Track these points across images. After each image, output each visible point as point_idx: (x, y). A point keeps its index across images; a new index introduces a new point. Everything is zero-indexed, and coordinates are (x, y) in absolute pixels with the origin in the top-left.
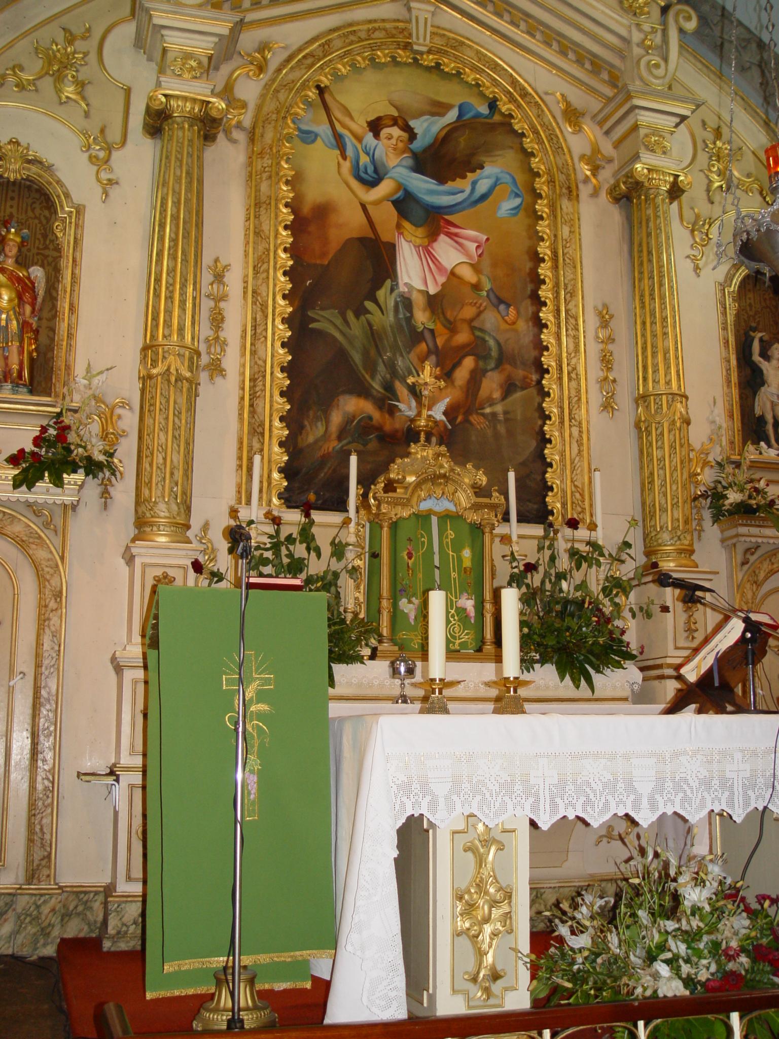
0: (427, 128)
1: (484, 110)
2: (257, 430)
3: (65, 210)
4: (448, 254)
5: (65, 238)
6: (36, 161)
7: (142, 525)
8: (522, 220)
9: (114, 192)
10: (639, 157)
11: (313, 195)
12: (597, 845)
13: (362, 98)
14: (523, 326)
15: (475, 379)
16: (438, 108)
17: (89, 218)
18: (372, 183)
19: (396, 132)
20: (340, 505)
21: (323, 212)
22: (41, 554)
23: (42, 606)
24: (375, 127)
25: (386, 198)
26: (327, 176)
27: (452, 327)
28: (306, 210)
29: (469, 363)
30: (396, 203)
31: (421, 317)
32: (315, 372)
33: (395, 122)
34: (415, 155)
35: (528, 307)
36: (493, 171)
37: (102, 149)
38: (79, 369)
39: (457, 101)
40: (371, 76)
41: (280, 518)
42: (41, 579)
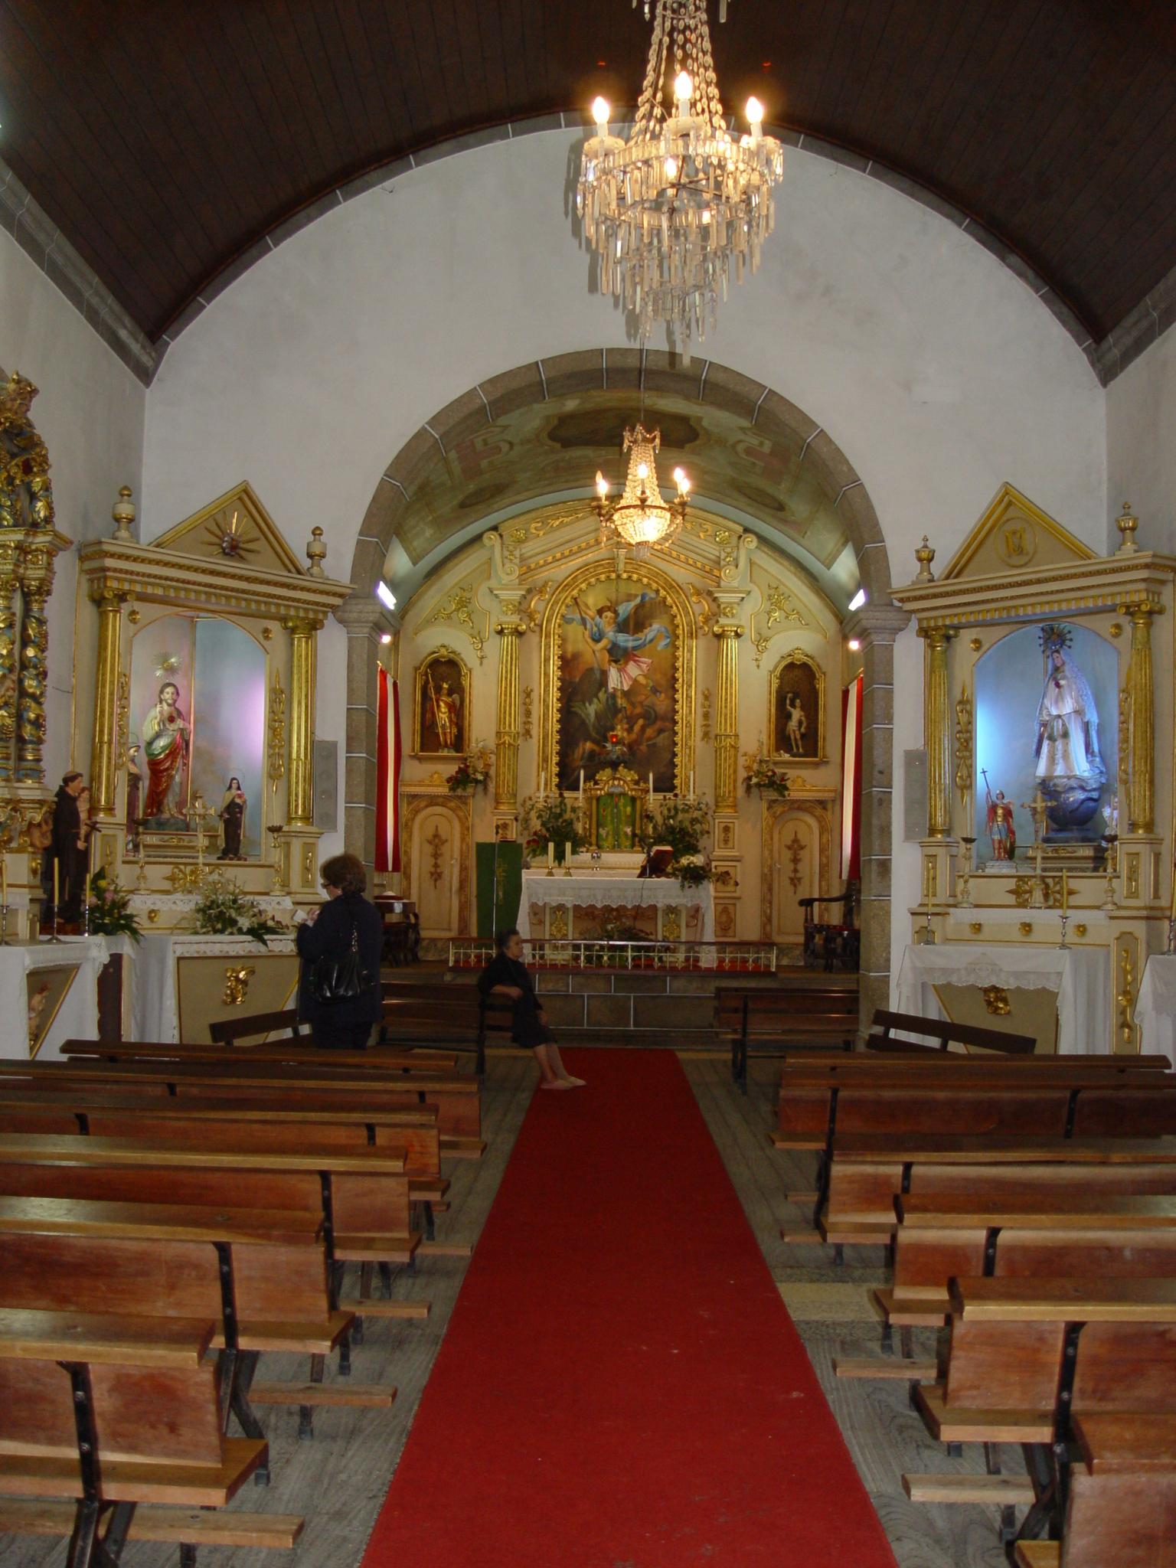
0: (625, 609)
1: (653, 595)
2: (545, 760)
3: (464, 671)
4: (633, 670)
5: (465, 683)
6: (453, 652)
7: (498, 802)
8: (670, 650)
9: (485, 661)
10: (352, 932)
11: (570, 649)
12: (258, 552)
13: (593, 600)
14: (667, 702)
15: (643, 729)
16: (629, 598)
17: (474, 673)
18: (597, 641)
19: (609, 614)
20: (577, 789)
21: (576, 656)
22: (461, 814)
23: (462, 834)
24: (600, 612)
25: (604, 648)
26: (579, 640)
27: (633, 704)
28: (569, 656)
29: (641, 722)
30: (610, 651)
31: (621, 702)
32: (570, 728)
33: (609, 609)
34: (618, 625)
35: (670, 692)
36: (656, 627)
37: (478, 637)
38: (473, 740)
39: (640, 593)
40: (599, 586)
41: (49, 593)
42: (462, 823)
